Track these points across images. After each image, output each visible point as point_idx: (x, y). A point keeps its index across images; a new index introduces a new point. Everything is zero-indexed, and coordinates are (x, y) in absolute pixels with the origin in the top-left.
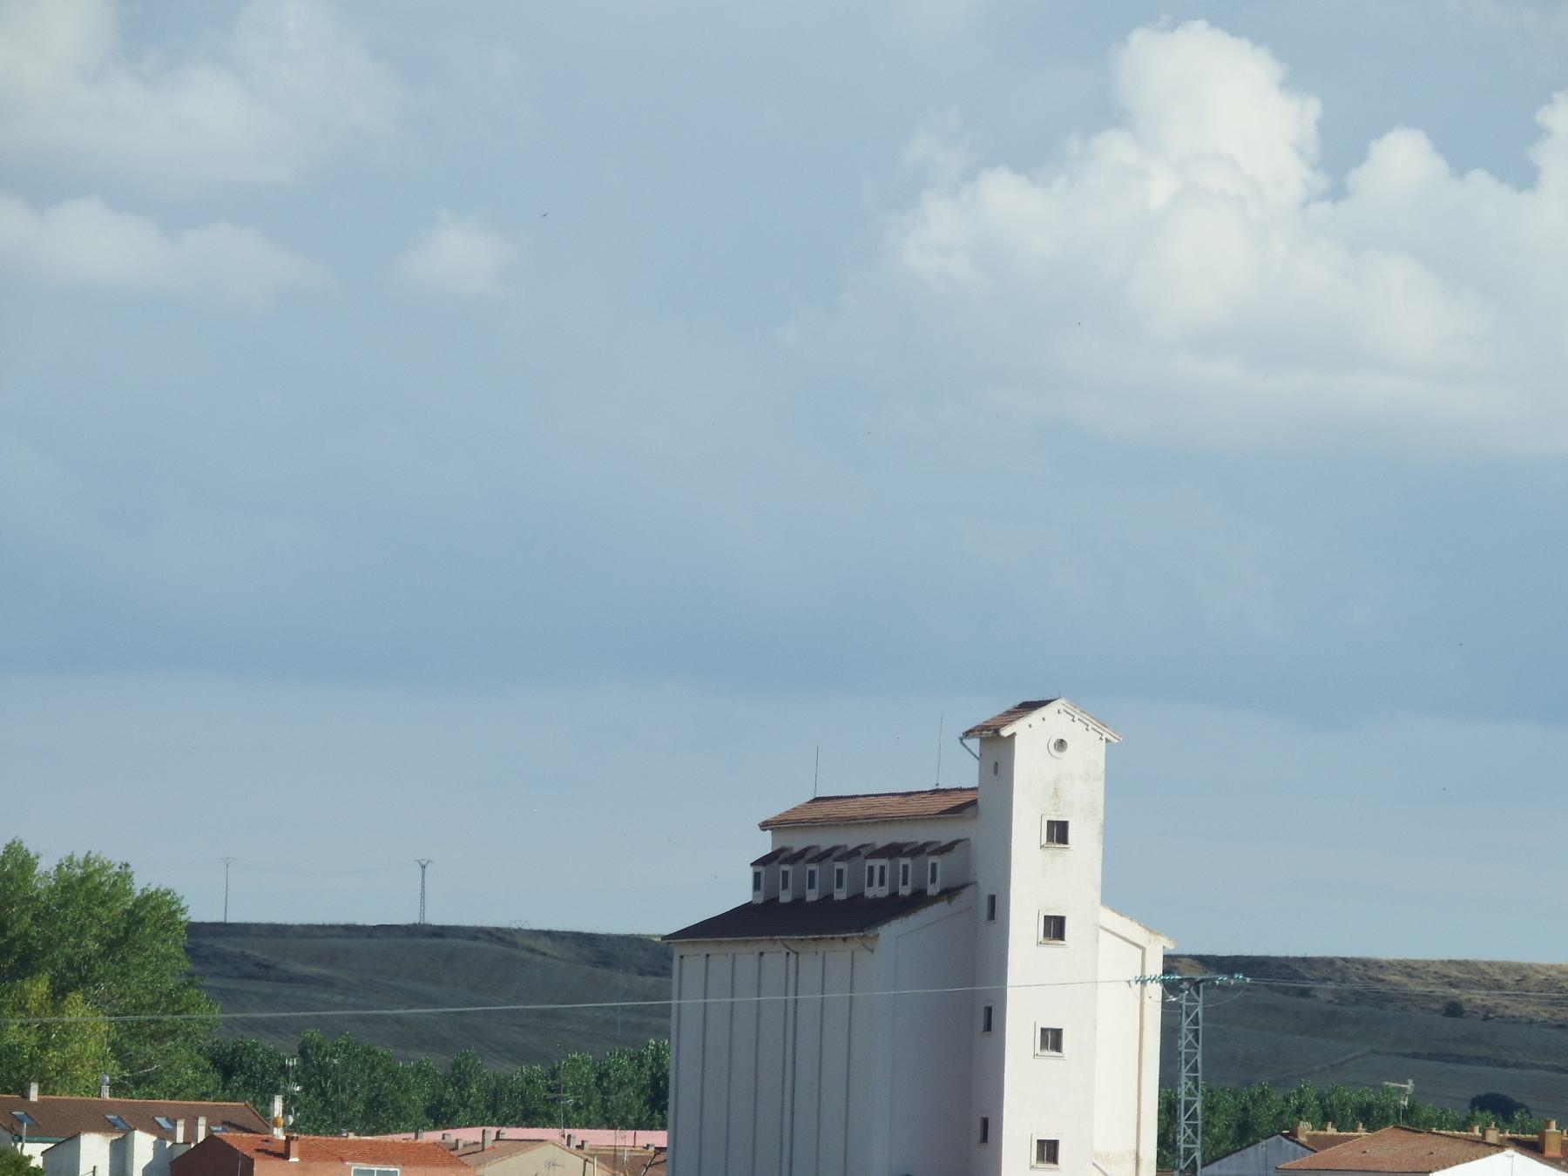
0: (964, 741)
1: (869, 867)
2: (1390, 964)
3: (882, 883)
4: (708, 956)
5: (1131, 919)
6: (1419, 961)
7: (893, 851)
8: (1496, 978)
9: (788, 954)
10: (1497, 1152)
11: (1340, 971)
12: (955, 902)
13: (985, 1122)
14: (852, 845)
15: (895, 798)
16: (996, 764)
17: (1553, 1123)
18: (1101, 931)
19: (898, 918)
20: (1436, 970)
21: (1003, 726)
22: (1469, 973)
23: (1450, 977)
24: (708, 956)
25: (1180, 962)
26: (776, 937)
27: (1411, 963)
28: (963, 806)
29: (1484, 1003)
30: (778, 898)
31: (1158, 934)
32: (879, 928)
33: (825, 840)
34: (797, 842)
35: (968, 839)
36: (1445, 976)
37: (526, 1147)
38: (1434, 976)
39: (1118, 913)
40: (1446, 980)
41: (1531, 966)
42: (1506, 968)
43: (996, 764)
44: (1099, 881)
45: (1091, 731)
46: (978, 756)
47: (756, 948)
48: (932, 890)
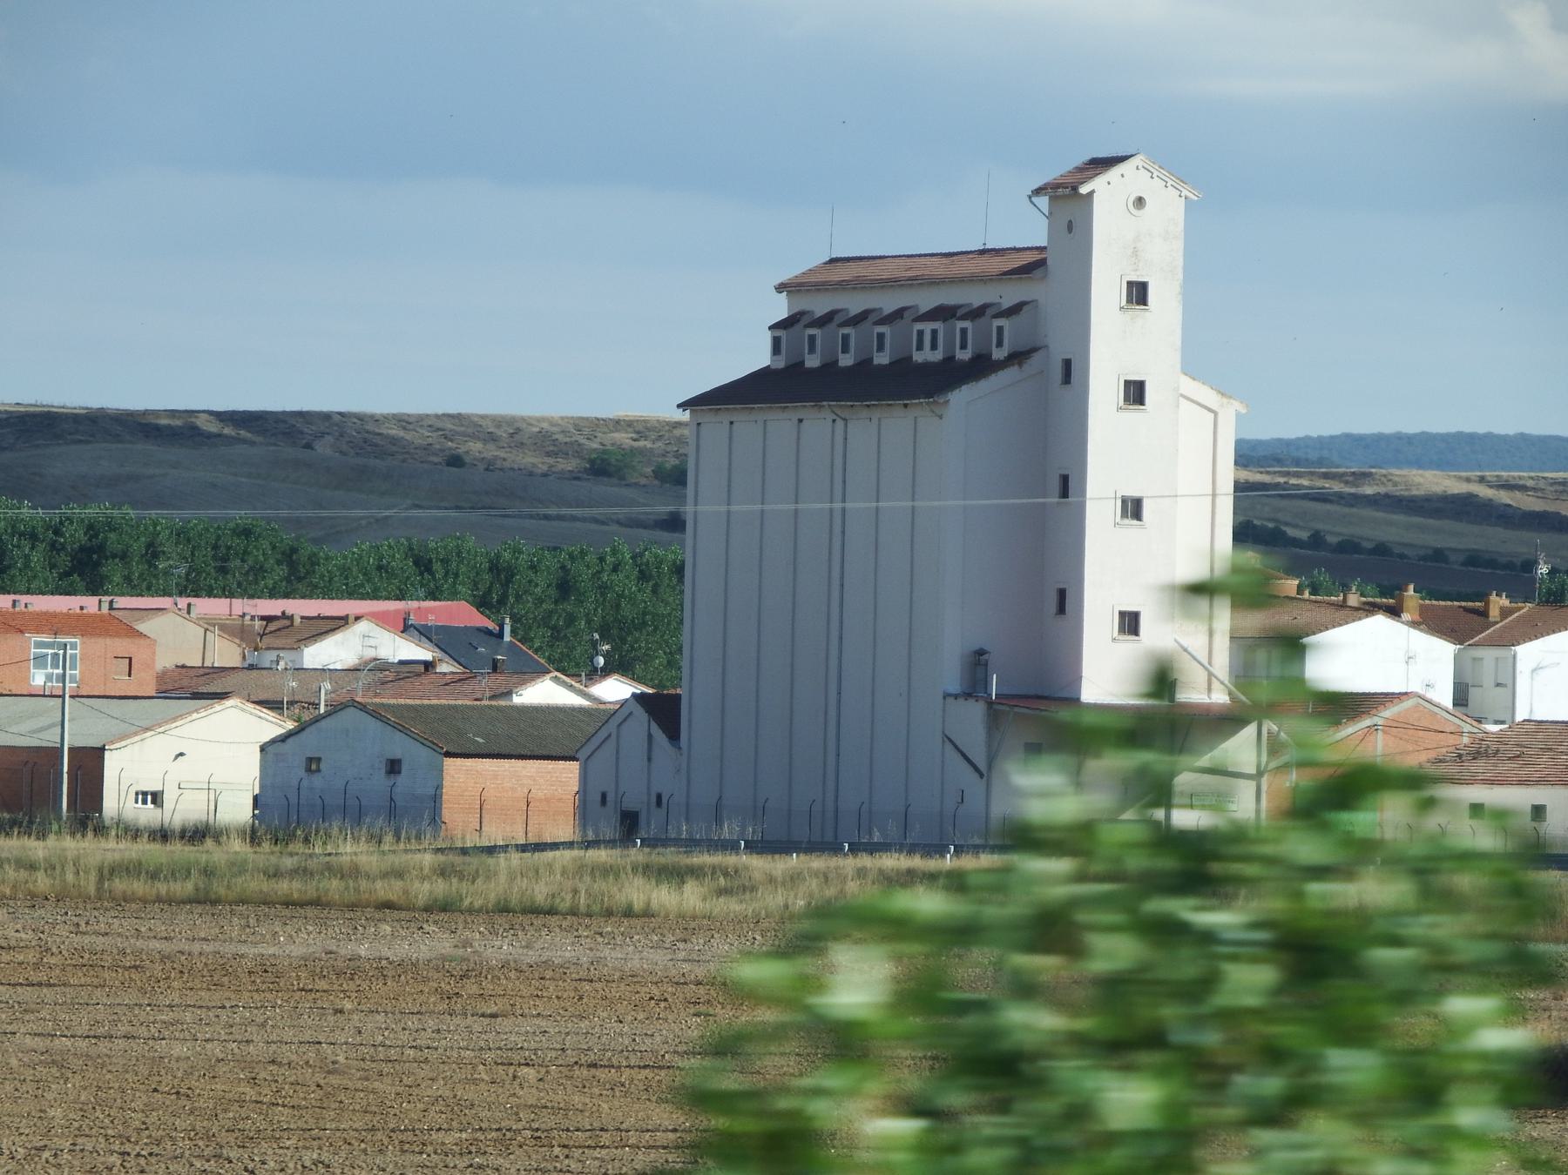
0: (1033, 199)
1: (878, 334)
2: (385, 417)
3: (934, 347)
4: (732, 423)
5: (1203, 383)
6: (412, 415)
7: (943, 313)
8: (489, 430)
9: (834, 421)
10: (1367, 616)
11: (337, 425)
12: (1026, 367)
13: (1062, 594)
14: (977, 303)
15: (934, 259)
16: (1070, 222)
17: (1411, 587)
18: (1181, 399)
19: (968, 383)
20: (430, 423)
21: (1082, 183)
22: (462, 425)
23: (444, 430)
24: (732, 423)
25: (196, 417)
26: (825, 403)
27: (406, 418)
28: (1033, 266)
29: (482, 456)
30: (803, 362)
31: (1230, 397)
32: (950, 393)
33: (854, 304)
34: (820, 305)
35: (1036, 301)
36: (438, 429)
37: (147, 616)
38: (429, 429)
39: (1190, 377)
40: (441, 433)
41: (523, 419)
42: (499, 421)
43: (1070, 222)
44: (1179, 343)
45: (1170, 188)
46: (1047, 214)
47: (795, 416)
48: (998, 354)
